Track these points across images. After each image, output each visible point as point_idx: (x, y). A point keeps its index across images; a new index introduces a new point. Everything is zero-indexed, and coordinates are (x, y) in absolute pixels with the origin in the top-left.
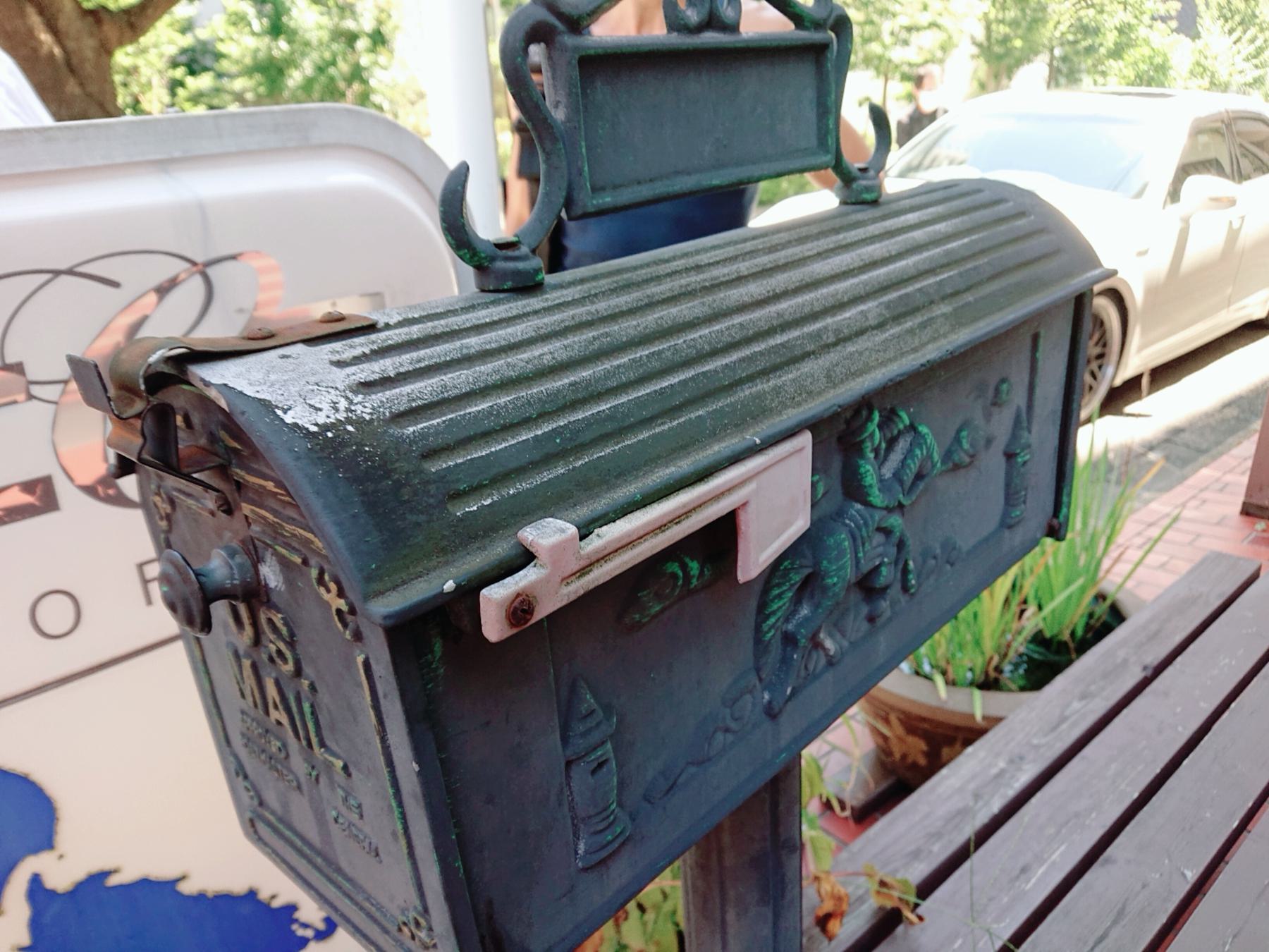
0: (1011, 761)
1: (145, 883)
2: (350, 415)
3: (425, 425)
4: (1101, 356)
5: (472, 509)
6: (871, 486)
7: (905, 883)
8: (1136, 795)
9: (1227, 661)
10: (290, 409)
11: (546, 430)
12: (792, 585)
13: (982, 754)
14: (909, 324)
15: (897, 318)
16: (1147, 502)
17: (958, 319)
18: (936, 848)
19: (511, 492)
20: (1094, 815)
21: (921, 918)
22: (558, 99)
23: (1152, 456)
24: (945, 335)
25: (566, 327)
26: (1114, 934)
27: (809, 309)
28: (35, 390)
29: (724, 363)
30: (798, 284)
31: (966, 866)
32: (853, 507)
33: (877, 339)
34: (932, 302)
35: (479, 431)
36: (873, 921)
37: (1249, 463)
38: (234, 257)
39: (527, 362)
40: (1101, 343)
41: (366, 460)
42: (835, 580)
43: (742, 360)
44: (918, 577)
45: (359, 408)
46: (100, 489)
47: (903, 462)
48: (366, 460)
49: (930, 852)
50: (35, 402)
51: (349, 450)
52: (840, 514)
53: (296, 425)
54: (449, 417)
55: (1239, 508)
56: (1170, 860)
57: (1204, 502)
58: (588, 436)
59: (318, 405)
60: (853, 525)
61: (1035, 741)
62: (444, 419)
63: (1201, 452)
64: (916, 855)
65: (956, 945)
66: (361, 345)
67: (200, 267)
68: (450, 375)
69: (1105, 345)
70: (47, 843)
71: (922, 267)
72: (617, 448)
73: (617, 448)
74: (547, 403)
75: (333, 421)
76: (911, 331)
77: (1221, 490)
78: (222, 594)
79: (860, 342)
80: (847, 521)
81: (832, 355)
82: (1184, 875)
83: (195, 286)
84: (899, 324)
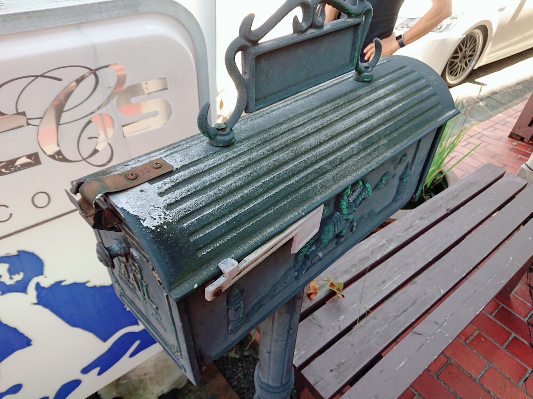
0: (388, 241)
1: (75, 284)
2: (165, 221)
3: (190, 222)
4: (471, 56)
5: (204, 254)
6: (344, 209)
7: (339, 284)
8: (431, 260)
9: (480, 211)
10: (145, 220)
11: (231, 219)
12: (310, 244)
13: (378, 237)
14: (369, 151)
15: (364, 149)
16: (472, 125)
17: (388, 146)
18: (354, 270)
19: (217, 245)
20: (413, 265)
21: (343, 296)
22: (246, 71)
23: (481, 103)
24: (382, 154)
25: (241, 168)
26: (410, 309)
27: (332, 150)
28: (30, 122)
29: (296, 180)
30: (330, 137)
31: (363, 278)
32: (336, 214)
33: (355, 160)
34: (380, 139)
35: (208, 223)
36: (327, 294)
37: (519, 114)
38: (107, 66)
39: (226, 188)
40: (473, 50)
41: (170, 240)
42: (325, 240)
43: (303, 177)
44: (357, 229)
45: (168, 217)
46: (56, 156)
47: (358, 196)
48: (170, 240)
49: (352, 271)
50: (30, 126)
51: (165, 236)
52: (332, 215)
53: (147, 227)
54: (198, 217)
55: (509, 134)
56: (437, 286)
57: (496, 129)
58: (245, 219)
59: (154, 217)
60: (335, 220)
61: (399, 234)
62: (196, 218)
63: (502, 104)
64: (346, 272)
65: (354, 306)
66: (168, 182)
67: (93, 71)
68: (199, 197)
69: (474, 51)
70: (41, 273)
71: (380, 122)
72: (254, 222)
73: (254, 222)
74: (232, 207)
75: (160, 224)
76: (369, 154)
77: (504, 125)
78: (117, 255)
79: (349, 162)
80: (333, 219)
81: (337, 169)
82: (440, 291)
83: (91, 79)
84: (365, 151)
